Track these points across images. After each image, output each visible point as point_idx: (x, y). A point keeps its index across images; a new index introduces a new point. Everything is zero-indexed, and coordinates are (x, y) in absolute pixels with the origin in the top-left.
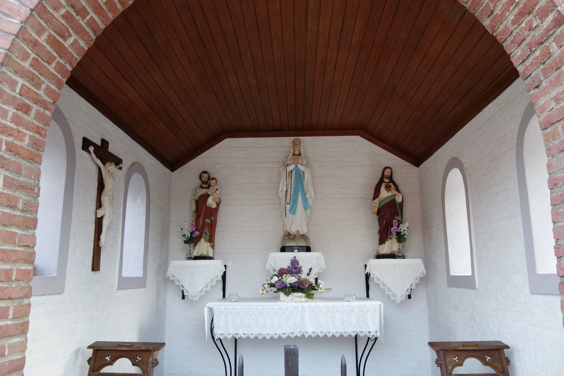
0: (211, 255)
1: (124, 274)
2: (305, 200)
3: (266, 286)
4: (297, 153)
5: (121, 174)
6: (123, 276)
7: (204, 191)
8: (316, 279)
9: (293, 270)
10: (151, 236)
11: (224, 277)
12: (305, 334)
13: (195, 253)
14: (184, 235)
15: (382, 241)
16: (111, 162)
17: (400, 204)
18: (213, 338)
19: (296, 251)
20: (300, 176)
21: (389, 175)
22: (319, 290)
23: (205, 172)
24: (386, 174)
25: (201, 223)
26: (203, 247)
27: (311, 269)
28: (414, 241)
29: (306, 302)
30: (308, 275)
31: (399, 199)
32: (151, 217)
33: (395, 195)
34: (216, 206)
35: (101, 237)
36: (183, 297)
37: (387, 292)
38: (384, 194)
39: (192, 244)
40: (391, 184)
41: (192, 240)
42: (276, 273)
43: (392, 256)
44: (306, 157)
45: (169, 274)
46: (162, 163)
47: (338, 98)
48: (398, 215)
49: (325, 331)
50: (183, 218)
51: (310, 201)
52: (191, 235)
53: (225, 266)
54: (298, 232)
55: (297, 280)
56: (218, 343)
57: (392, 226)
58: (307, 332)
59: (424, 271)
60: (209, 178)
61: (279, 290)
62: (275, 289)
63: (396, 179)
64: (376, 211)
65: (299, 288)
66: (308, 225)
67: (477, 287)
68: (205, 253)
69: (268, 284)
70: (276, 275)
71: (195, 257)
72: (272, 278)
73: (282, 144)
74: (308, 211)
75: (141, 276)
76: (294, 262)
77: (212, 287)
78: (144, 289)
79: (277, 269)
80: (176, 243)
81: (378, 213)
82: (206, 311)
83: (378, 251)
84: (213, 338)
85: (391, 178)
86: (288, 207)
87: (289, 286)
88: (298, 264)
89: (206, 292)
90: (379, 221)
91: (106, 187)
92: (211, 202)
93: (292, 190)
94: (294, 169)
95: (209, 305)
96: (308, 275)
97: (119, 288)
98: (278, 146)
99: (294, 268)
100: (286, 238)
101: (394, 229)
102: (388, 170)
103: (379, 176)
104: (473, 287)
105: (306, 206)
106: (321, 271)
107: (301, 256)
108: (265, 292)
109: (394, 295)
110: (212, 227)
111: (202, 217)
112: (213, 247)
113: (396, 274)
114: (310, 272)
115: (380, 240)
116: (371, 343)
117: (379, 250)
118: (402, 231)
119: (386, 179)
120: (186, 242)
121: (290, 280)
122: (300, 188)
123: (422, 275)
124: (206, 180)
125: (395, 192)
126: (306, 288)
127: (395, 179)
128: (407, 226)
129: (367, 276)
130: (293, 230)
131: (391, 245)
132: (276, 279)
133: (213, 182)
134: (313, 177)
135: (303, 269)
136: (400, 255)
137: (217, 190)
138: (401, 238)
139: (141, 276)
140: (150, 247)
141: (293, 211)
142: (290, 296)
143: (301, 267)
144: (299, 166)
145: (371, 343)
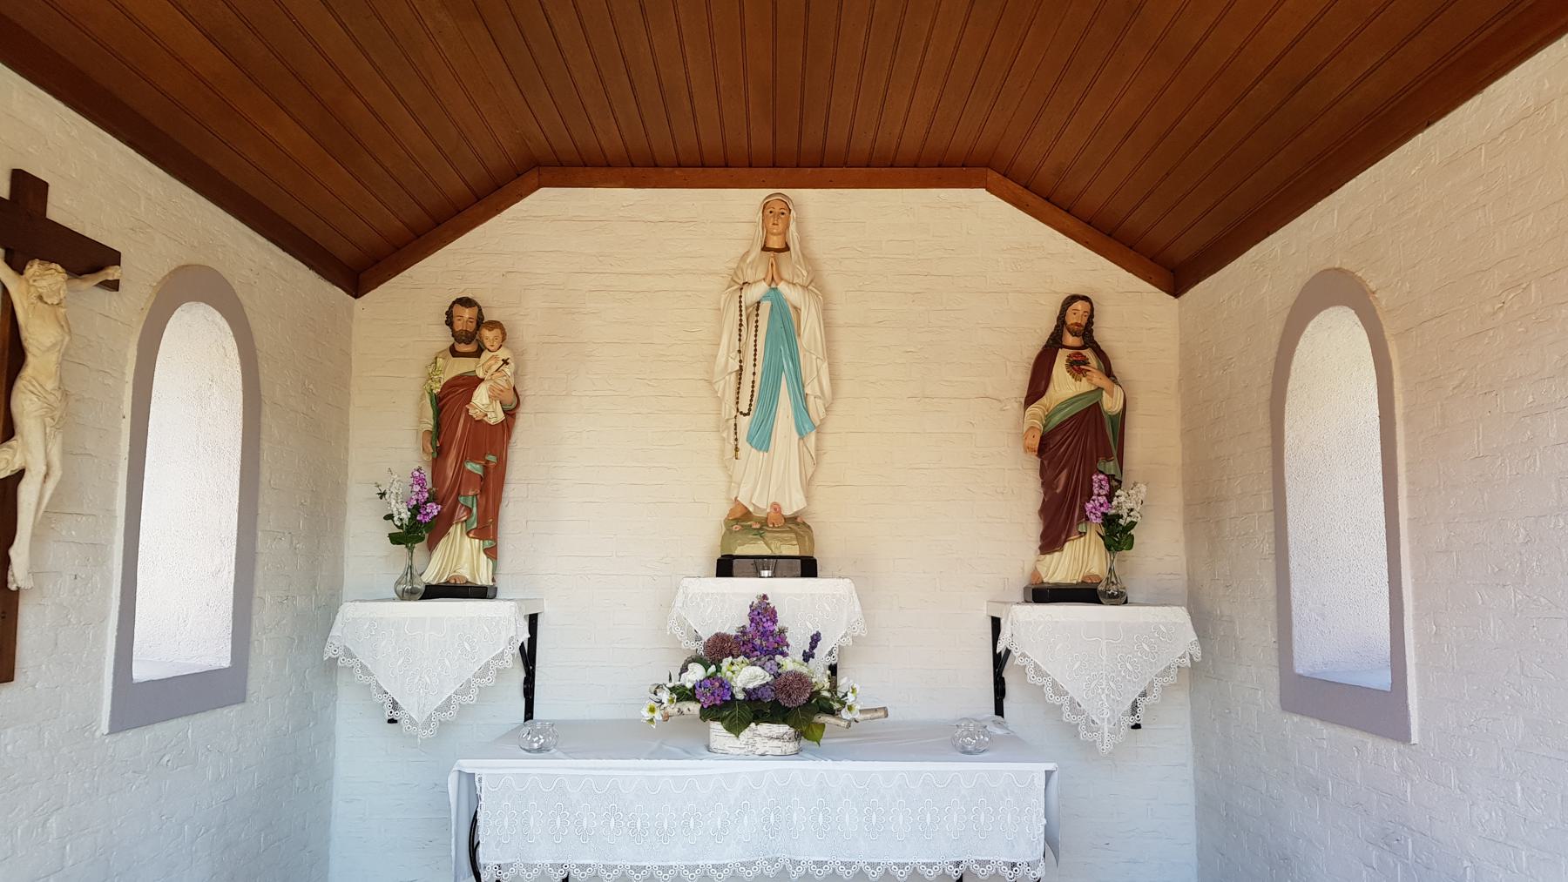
0: (483, 579)
1: (140, 673)
2: (801, 400)
3: (665, 696)
4: (775, 242)
5: (110, 314)
7: (462, 366)
8: (833, 669)
9: (757, 642)
10: (267, 521)
11: (528, 656)
12: (790, 868)
13: (432, 574)
14: (389, 517)
15: (1051, 541)
16: (48, 258)
17: (1113, 418)
19: (765, 573)
21: (1084, 321)
22: (845, 714)
23: (466, 302)
24: (1072, 319)
25: (450, 473)
26: (458, 555)
27: (815, 639)
28: (1161, 545)
30: (807, 657)
31: (1111, 404)
32: (266, 455)
33: (1100, 389)
34: (501, 416)
35: (12, 552)
37: (1067, 716)
38: (1064, 386)
39: (419, 547)
40: (1088, 353)
41: (417, 531)
43: (1085, 593)
44: (807, 259)
45: (329, 652)
46: (311, 267)
47: (926, 49)
48: (1108, 458)
50: (388, 450)
51: (816, 407)
52: (413, 517)
53: (533, 620)
54: (776, 507)
55: (769, 678)
57: (1089, 495)
59: (1197, 652)
60: (480, 322)
61: (709, 713)
62: (695, 708)
63: (1105, 333)
64: (1036, 443)
66: (808, 485)
67: (1415, 738)
69: (672, 690)
71: (428, 587)
72: (684, 669)
73: (736, 209)
74: (812, 437)
75: (226, 663)
76: (763, 613)
78: (239, 707)
79: (706, 635)
80: (367, 548)
81: (1042, 450)
83: (1035, 573)
86: (744, 422)
87: (740, 696)
88: (775, 622)
90: (1042, 474)
91: (30, 359)
92: (482, 402)
94: (765, 297)
95: (467, 765)
96: (807, 657)
97: (119, 724)
99: (761, 635)
100: (737, 527)
103: (1047, 326)
104: (1401, 734)
105: (805, 424)
106: (848, 641)
107: (786, 592)
108: (658, 716)
110: (491, 486)
111: (453, 453)
112: (492, 553)
114: (813, 647)
115: (1044, 536)
117: (1042, 570)
118: (1124, 512)
119: (1074, 337)
120: (395, 539)
121: (746, 676)
122: (787, 364)
123: (1187, 662)
124: (470, 329)
125: (1099, 379)
126: (799, 708)
127: (1102, 334)
128: (1142, 496)
129: (999, 661)
130: (759, 502)
131: (1081, 558)
132: (696, 673)
133: (488, 335)
134: (827, 325)
136: (1113, 590)
137: (505, 362)
138: (1117, 535)
139: (226, 663)
140: (262, 560)
141: (762, 440)
142: (746, 734)
143: (782, 631)
144: (783, 287)
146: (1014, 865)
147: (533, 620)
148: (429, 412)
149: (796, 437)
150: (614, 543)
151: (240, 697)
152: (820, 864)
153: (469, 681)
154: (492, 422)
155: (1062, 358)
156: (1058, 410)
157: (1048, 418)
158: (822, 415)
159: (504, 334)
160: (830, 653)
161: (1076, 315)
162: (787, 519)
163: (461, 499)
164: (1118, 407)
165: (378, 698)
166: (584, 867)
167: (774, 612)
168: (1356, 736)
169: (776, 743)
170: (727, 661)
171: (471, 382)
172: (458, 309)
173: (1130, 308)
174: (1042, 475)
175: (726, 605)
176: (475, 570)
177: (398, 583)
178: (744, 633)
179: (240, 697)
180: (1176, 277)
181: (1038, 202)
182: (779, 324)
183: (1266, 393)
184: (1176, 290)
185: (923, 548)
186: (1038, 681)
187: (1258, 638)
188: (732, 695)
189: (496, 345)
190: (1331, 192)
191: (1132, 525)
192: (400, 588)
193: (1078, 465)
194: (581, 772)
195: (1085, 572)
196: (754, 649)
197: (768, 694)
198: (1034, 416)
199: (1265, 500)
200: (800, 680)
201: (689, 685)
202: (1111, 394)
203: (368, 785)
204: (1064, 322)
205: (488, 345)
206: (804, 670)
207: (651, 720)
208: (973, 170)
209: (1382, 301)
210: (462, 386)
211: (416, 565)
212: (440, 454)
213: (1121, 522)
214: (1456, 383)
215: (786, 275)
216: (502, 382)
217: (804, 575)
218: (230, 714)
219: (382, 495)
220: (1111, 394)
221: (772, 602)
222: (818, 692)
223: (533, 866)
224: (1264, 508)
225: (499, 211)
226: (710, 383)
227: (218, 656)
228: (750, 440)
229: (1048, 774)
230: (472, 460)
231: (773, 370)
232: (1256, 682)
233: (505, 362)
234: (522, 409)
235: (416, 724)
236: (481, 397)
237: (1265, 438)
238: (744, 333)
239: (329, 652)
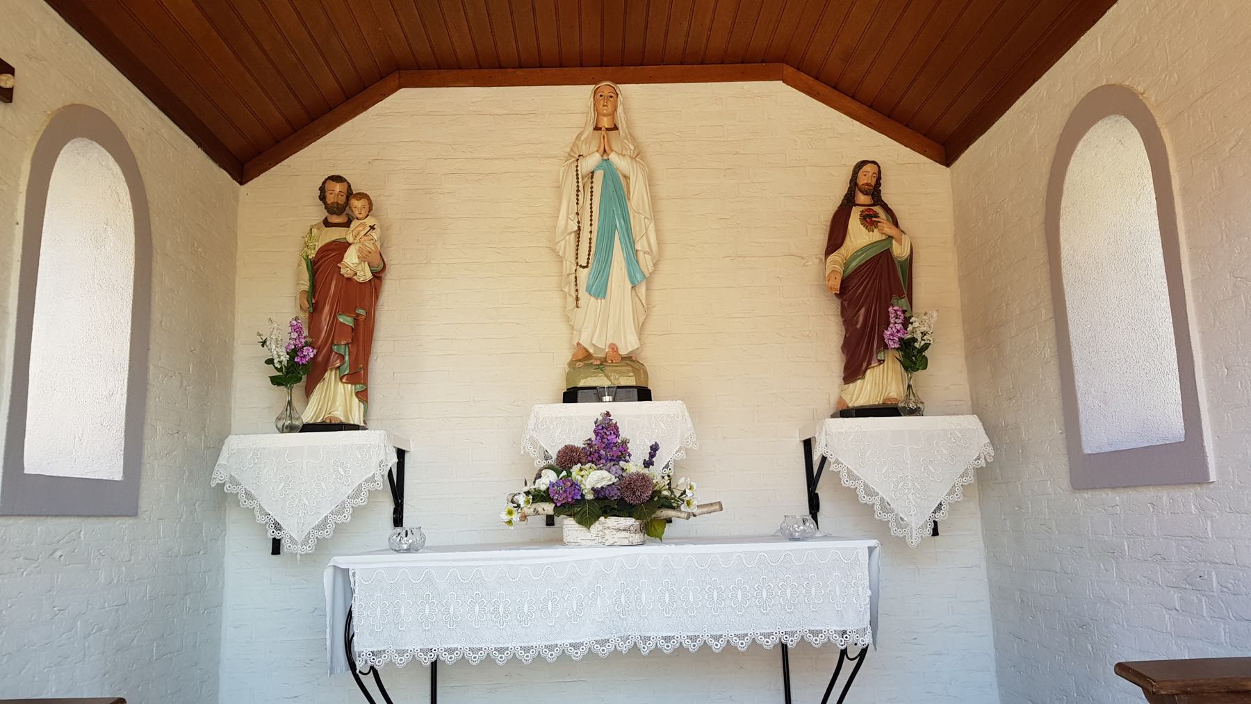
0: (356, 419)
3: (521, 499)
6: (29, 469)
7: (335, 234)
9: (602, 452)
12: (641, 645)
13: (309, 415)
14: (270, 361)
15: (853, 372)
17: (902, 264)
18: (352, 666)
20: (617, 190)
23: (338, 179)
24: (863, 180)
26: (334, 396)
27: (654, 449)
28: (947, 370)
29: (643, 544)
30: (647, 464)
32: (156, 299)
33: (890, 237)
34: (369, 276)
36: (276, 547)
37: (879, 514)
38: (859, 237)
39: (298, 389)
40: (877, 209)
41: (297, 373)
42: (552, 462)
44: (633, 139)
45: (219, 475)
46: (199, 145)
48: (901, 296)
49: (705, 634)
50: (270, 307)
51: (646, 262)
53: (401, 454)
54: (614, 348)
56: (369, 682)
58: (646, 639)
60: (350, 194)
62: (549, 508)
64: (837, 284)
65: (621, 501)
66: (641, 330)
68: (339, 415)
70: (550, 467)
72: (539, 476)
73: (572, 101)
74: (642, 290)
75: (118, 477)
76: (606, 428)
77: (356, 510)
78: (131, 521)
79: (553, 453)
80: (252, 391)
82: (328, 575)
84: (352, 666)
85: (875, 191)
86: (583, 273)
87: (589, 497)
88: (617, 436)
89: (321, 543)
93: (595, 228)
94: (598, 167)
95: (342, 561)
98: (556, 111)
99: (606, 445)
101: (892, 333)
102: (868, 168)
104: (1200, 477)
106: (682, 455)
107: (626, 413)
108: (516, 517)
109: (900, 522)
110: (361, 338)
111: (327, 309)
112: (363, 396)
113: (908, 460)
114: (652, 455)
115: (846, 368)
116: (848, 667)
119: (864, 195)
120: (275, 381)
121: (593, 478)
124: (340, 202)
125: (889, 229)
126: (644, 505)
127: (888, 195)
130: (596, 340)
132: (549, 477)
133: (357, 204)
134: (654, 199)
135: (631, 448)
137: (372, 228)
139: (118, 477)
141: (600, 289)
142: (596, 527)
143: (625, 442)
144: (613, 157)
145: (848, 667)
146: (844, 632)
147: (401, 454)
148: (306, 276)
149: (629, 286)
150: (472, 376)
151: (131, 511)
152: (668, 639)
153: (343, 502)
154: (361, 280)
155: (855, 214)
156: (854, 257)
157: (846, 265)
158: (651, 268)
159: (371, 204)
160: (667, 466)
161: (865, 178)
162: (623, 358)
163: (335, 348)
164: (906, 253)
165: (261, 519)
166: (451, 651)
167: (617, 428)
168: (1149, 494)
169: (623, 534)
170: (575, 469)
171: (342, 246)
172: (330, 184)
173: (908, 173)
174: (843, 314)
175: (578, 424)
176: (348, 411)
177: (279, 419)
178: (590, 445)
179: (131, 511)
180: (946, 149)
181: (826, 90)
182: (611, 188)
183: (1039, 218)
184: (947, 158)
185: (741, 373)
186: (851, 484)
187: (1043, 431)
188: (582, 496)
189: (364, 213)
190: (1094, 22)
191: (926, 346)
192: (280, 426)
193: (873, 307)
194: (448, 564)
195: (884, 395)
196: (600, 457)
197: (615, 494)
198: (835, 262)
199: (1044, 311)
200: (644, 479)
201: (543, 488)
202: (900, 242)
203: (258, 609)
204: (856, 184)
205: (356, 213)
206: (646, 471)
207: (510, 522)
208: (771, 65)
209: (1151, 99)
210: (333, 250)
211: (295, 403)
212: (315, 310)
213: (917, 345)
214: (1231, 145)
215: (614, 147)
216: (370, 246)
217: (640, 399)
218: (121, 526)
219: (264, 343)
220: (900, 242)
221: (614, 419)
222: (660, 492)
223: (404, 652)
224: (1044, 318)
225: (365, 108)
226: (553, 250)
227: (113, 470)
228: (589, 290)
229: (871, 550)
230: (344, 313)
231: (607, 223)
232: (1047, 473)
233: (372, 228)
234: (389, 288)
235: (295, 543)
236: (351, 258)
237: (1042, 257)
238: (581, 202)
239: (219, 475)
